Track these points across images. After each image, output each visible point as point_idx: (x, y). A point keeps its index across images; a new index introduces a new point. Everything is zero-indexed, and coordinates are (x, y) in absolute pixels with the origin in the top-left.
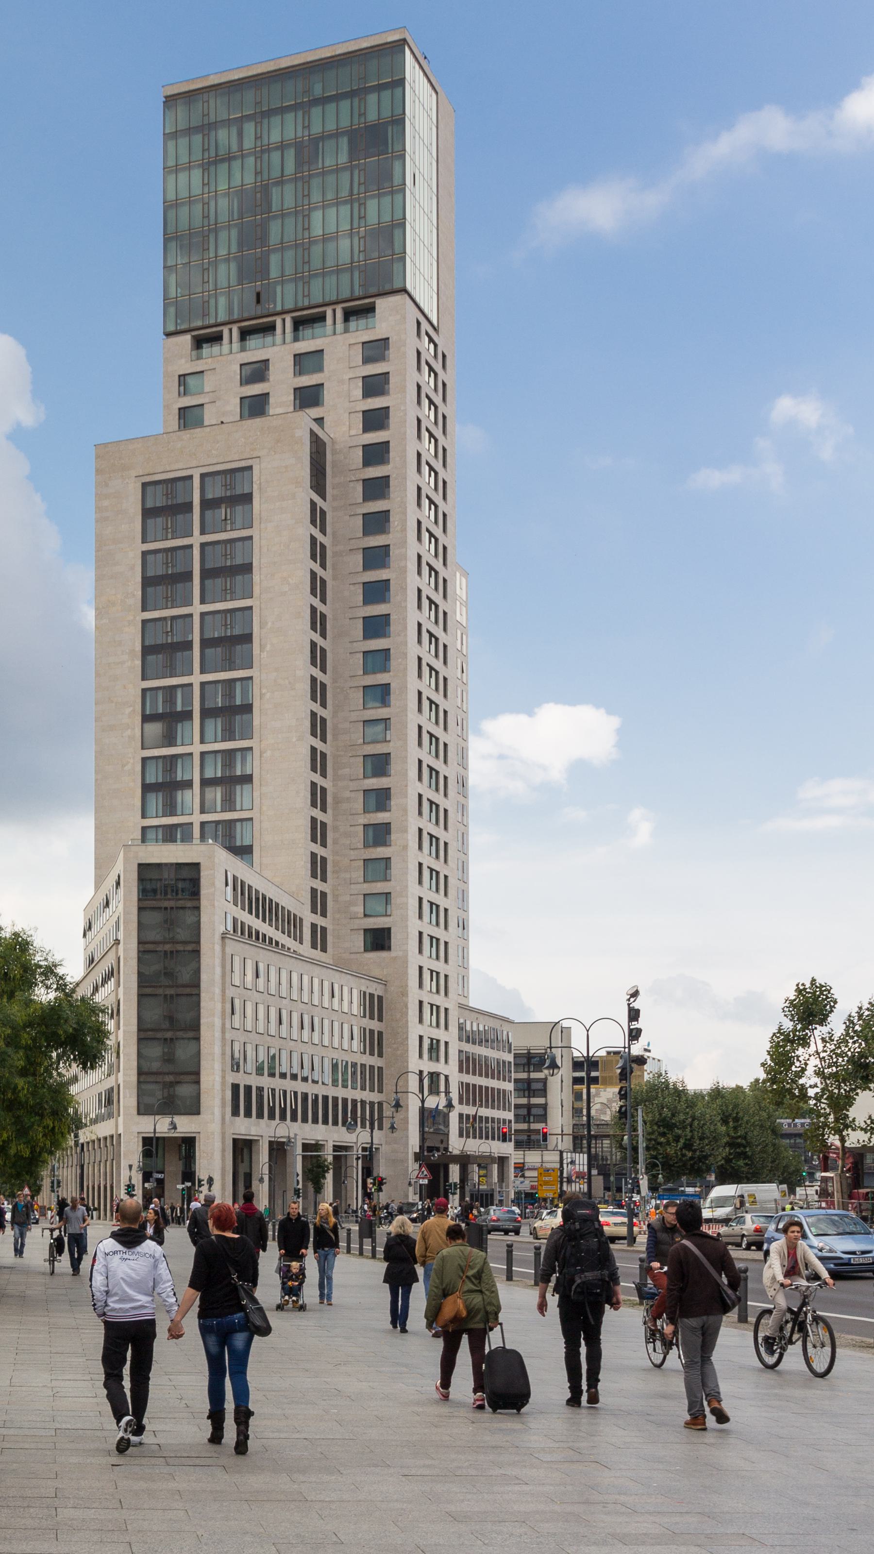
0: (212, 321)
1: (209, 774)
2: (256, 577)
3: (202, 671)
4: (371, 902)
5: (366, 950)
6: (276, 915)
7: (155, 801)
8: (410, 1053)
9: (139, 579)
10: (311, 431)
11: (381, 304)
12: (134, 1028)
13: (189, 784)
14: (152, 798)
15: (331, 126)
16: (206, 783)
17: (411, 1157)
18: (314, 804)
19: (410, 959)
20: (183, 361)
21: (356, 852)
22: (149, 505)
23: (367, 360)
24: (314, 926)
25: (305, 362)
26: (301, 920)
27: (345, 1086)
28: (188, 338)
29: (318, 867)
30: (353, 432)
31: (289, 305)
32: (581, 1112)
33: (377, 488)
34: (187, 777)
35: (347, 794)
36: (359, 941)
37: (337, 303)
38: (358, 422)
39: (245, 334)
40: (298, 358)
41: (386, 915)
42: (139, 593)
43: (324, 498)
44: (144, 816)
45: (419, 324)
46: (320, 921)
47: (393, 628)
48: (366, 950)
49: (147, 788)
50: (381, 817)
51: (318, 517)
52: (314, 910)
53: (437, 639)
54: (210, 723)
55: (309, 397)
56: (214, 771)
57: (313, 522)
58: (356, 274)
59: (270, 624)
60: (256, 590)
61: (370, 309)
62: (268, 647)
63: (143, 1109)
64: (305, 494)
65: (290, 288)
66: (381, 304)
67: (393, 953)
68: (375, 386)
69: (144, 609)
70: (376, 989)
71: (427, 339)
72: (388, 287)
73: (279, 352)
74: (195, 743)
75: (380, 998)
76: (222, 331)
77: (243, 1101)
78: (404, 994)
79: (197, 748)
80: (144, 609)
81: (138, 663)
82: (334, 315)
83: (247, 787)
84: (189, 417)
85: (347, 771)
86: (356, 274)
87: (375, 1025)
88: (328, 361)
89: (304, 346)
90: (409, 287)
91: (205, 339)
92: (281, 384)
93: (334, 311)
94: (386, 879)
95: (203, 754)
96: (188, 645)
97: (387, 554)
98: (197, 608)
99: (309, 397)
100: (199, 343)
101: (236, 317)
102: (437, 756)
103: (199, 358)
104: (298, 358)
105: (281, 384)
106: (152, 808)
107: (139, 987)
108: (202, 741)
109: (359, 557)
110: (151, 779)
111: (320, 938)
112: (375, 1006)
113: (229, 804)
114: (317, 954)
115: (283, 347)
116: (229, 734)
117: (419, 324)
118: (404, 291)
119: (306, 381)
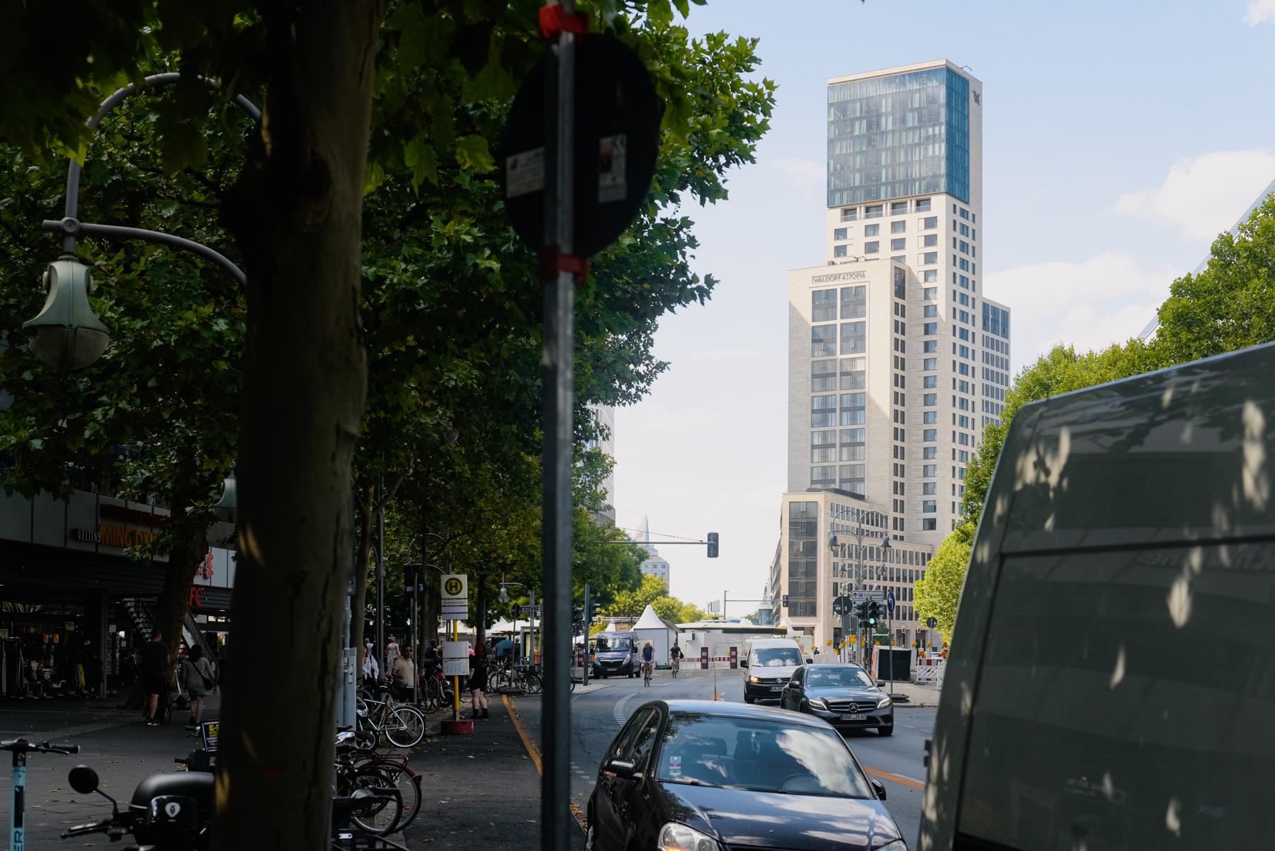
1: (844, 477)
13: (834, 410)
16: (842, 445)
24: (895, 519)
25: (896, 226)
27: (911, 563)
29: (899, 488)
32: (938, 119)
40: (893, 241)
49: (814, 376)
54: (845, 414)
55: (898, 244)
56: (847, 439)
68: (931, 240)
74: (837, 424)
79: (838, 428)
82: (911, 205)
84: (840, 251)
91: (848, 213)
92: (885, 237)
99: (898, 244)
100: (846, 212)
103: (845, 220)
105: (885, 237)
119: (897, 236)
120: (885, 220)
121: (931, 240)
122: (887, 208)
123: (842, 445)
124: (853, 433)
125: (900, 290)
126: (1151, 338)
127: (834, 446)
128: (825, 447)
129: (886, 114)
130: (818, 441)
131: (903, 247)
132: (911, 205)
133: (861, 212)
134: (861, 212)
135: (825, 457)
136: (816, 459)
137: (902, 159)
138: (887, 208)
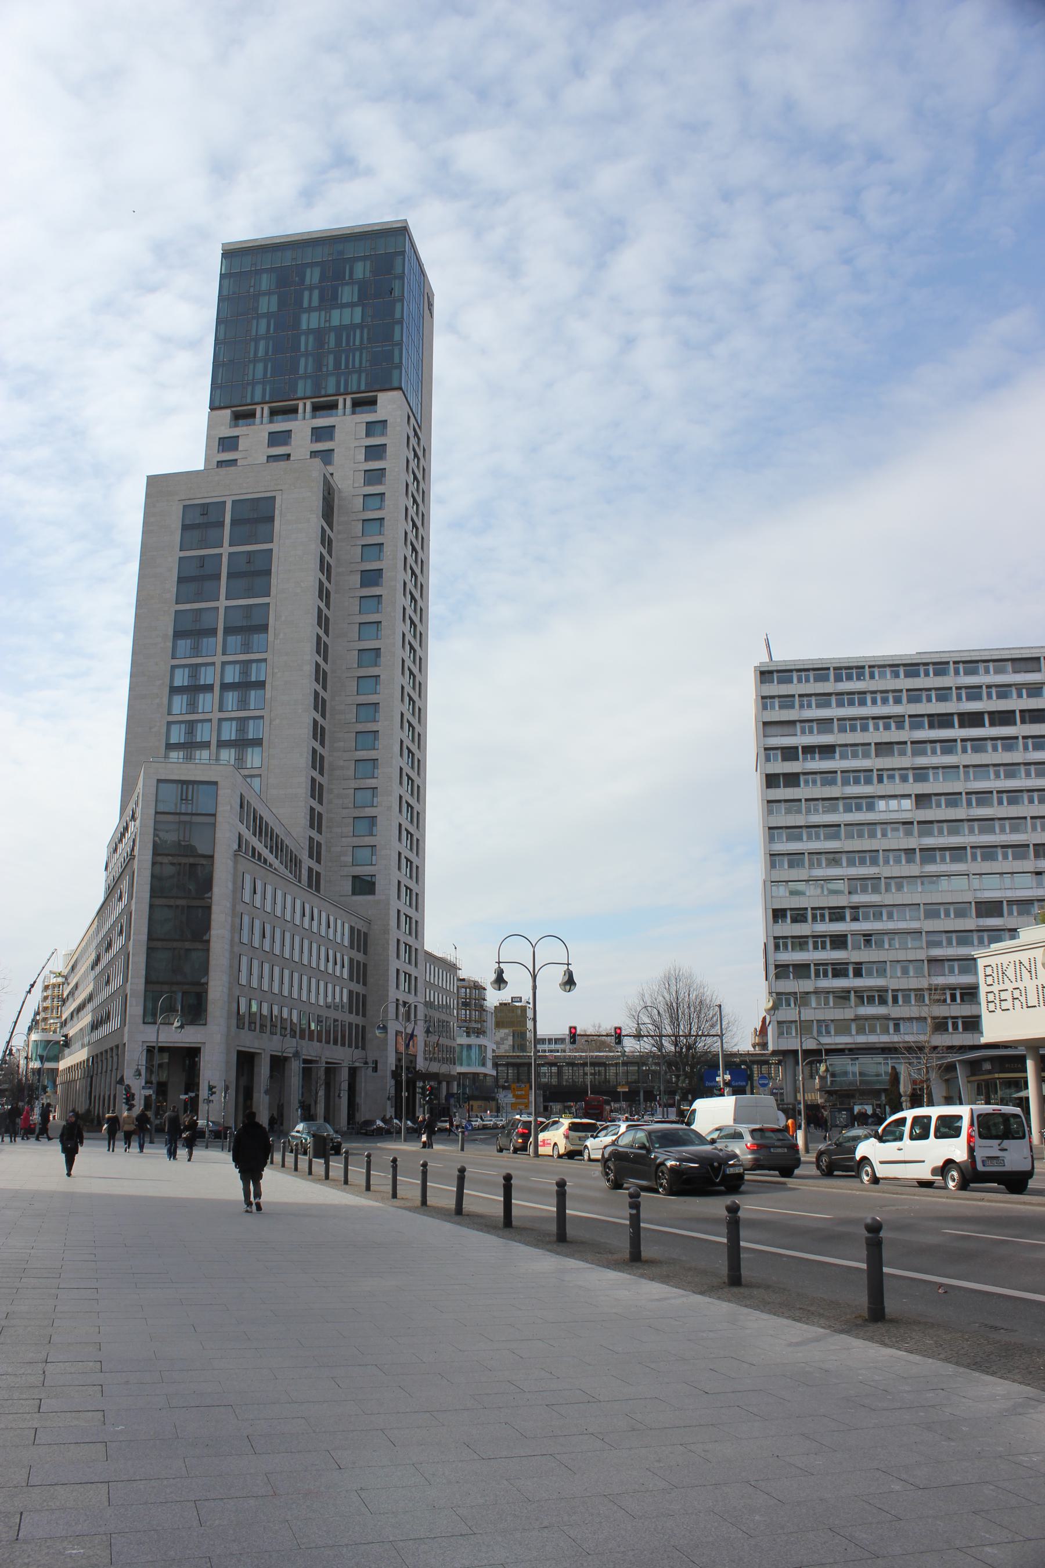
0: (249, 401)
2: (274, 581)
4: (369, 500)
5: (354, 893)
8: (390, 983)
10: (322, 527)
11: (382, 398)
12: (144, 937)
15: (347, 311)
17: (389, 1074)
18: (312, 826)
19: (392, 902)
20: (223, 428)
21: (347, 811)
22: (187, 522)
24: (310, 870)
25: (321, 434)
28: (228, 412)
30: (356, 485)
31: (308, 394)
35: (341, 763)
36: (348, 886)
39: (273, 413)
41: (372, 865)
43: (327, 635)
45: (409, 417)
46: (316, 867)
48: (354, 893)
52: (311, 856)
53: (412, 808)
54: (231, 639)
56: (232, 675)
57: (316, 708)
58: (363, 376)
59: (283, 618)
61: (373, 402)
62: (281, 636)
63: (150, 1016)
65: (315, 315)
66: (382, 398)
67: (376, 897)
68: (375, 452)
70: (360, 925)
71: (411, 523)
72: (387, 386)
75: (365, 934)
76: (255, 410)
77: (242, 1021)
78: (386, 931)
82: (345, 402)
83: (257, 750)
85: (341, 744)
86: (363, 376)
87: (359, 957)
88: (338, 434)
89: (321, 422)
91: (244, 416)
92: (301, 443)
93: (345, 400)
94: (376, 665)
97: (381, 576)
98: (226, 550)
101: (267, 399)
102: (411, 849)
103: (236, 426)
105: (301, 443)
106: (180, 652)
107: (151, 897)
110: (177, 683)
112: (360, 940)
113: (243, 704)
115: (303, 422)
116: (247, 648)
117: (409, 417)
118: (401, 389)
120: (301, 427)
121: (375, 452)
122: (305, 407)
123: (222, 744)
124: (242, 723)
125: (328, 513)
126: (257, 1120)
127: (209, 688)
128: (194, 689)
129: (311, 289)
130: (181, 679)
131: (331, 438)
132: (345, 402)
133: (263, 411)
134: (263, 411)
135: (192, 707)
136: (176, 709)
137: (332, 344)
138: (305, 407)
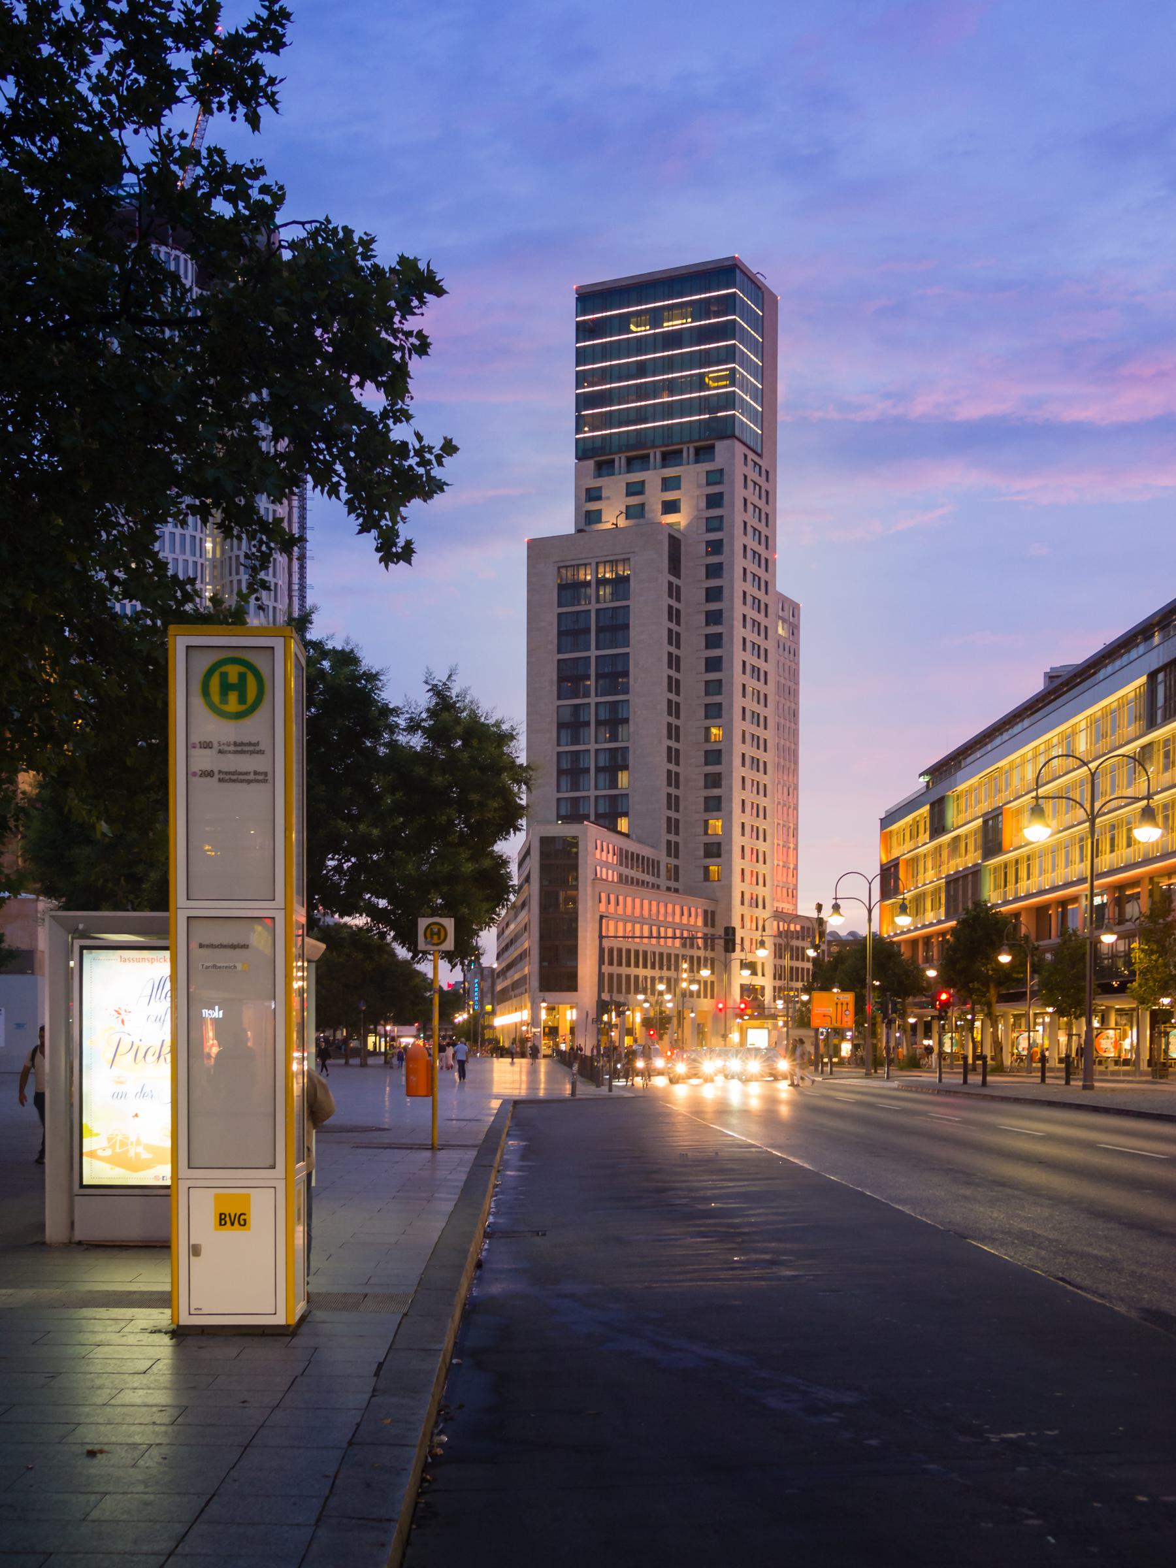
2: (632, 633)
3: (597, 648)
6: (641, 416)
7: (566, 735)
9: (556, 631)
14: (563, 733)
23: (708, 530)
26: (658, 862)
33: (714, 571)
34: (586, 719)
37: (691, 442)
38: (702, 618)
42: (556, 641)
44: (558, 791)
47: (725, 548)
49: (560, 772)
50: (715, 792)
51: (674, 592)
60: (632, 642)
64: (666, 577)
69: (559, 652)
73: (652, 478)
74: (593, 744)
79: (593, 747)
80: (559, 652)
81: (555, 688)
83: (625, 726)
90: (737, 433)
95: (597, 751)
96: (588, 630)
98: (593, 653)
103: (600, 476)
104: (664, 480)
106: (564, 787)
108: (596, 788)
109: (703, 617)
110: (564, 766)
111: (674, 873)
113: (614, 738)
114: (672, 884)
